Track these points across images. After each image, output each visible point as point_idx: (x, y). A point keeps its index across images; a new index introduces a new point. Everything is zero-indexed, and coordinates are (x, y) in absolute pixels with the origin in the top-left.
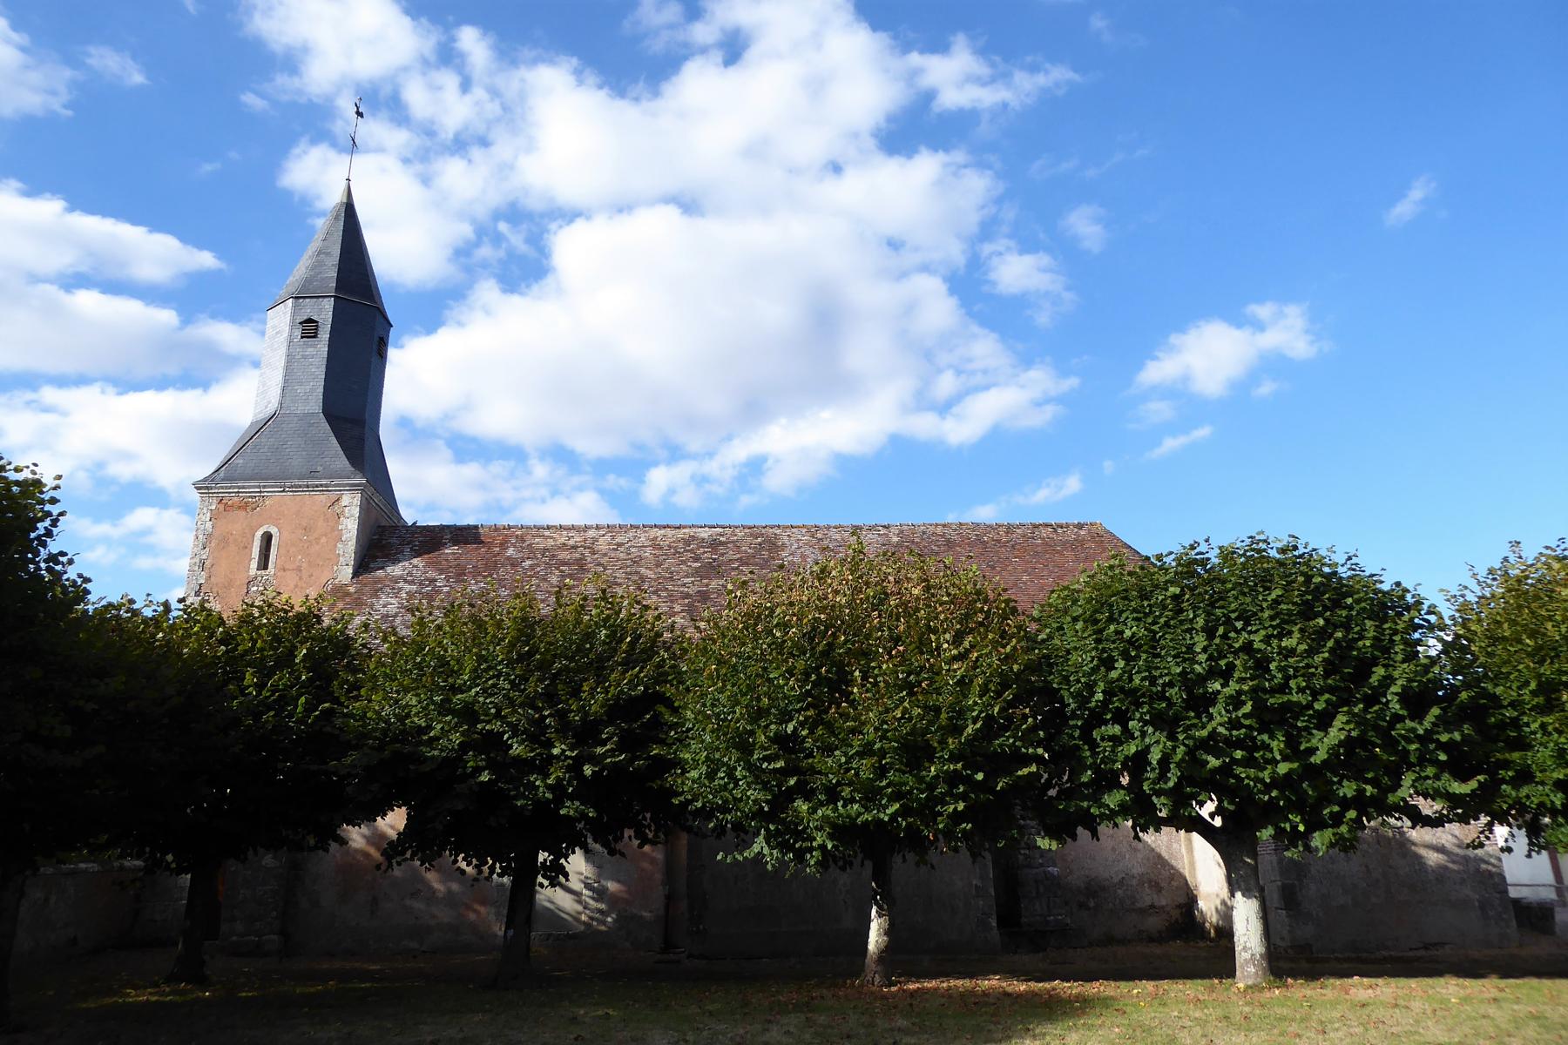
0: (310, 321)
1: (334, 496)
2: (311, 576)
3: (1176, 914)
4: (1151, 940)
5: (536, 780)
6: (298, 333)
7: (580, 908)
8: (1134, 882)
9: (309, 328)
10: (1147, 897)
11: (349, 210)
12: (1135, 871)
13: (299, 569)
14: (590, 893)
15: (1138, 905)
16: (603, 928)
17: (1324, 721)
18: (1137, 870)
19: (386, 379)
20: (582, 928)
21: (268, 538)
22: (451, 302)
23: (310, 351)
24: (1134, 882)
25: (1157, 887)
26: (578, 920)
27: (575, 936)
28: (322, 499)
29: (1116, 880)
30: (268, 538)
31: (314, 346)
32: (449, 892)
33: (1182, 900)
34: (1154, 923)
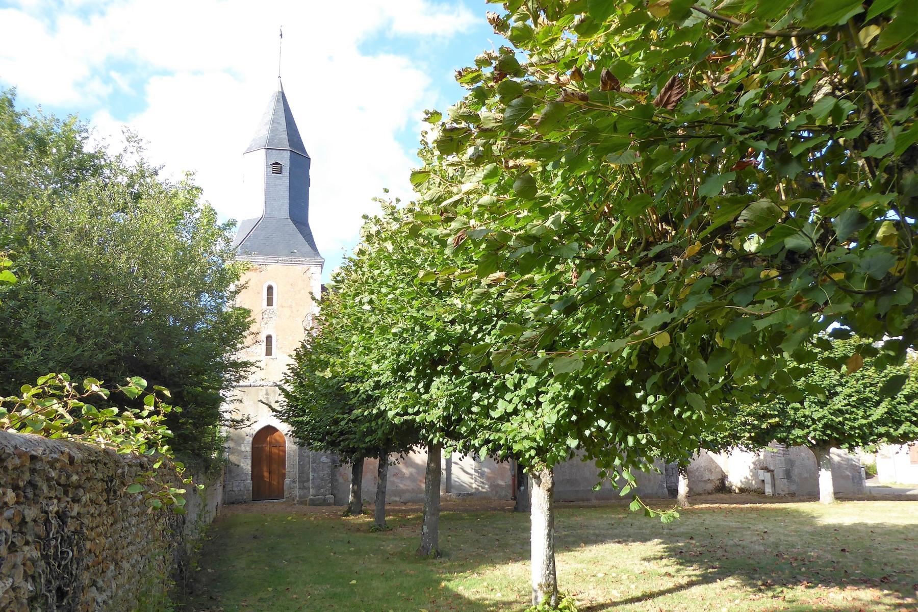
0: (277, 164)
1: (306, 267)
2: (298, 311)
3: (718, 483)
4: (709, 493)
5: (813, 155)
6: (271, 170)
7: (473, 481)
8: (702, 469)
9: (276, 167)
10: (707, 476)
11: (282, 98)
12: (702, 465)
13: (291, 307)
14: (477, 474)
15: (704, 479)
16: (484, 490)
17: (878, 404)
18: (703, 464)
19: (311, 190)
20: (474, 490)
21: (270, 288)
22: (582, 544)
23: (278, 182)
24: (702, 469)
25: (711, 471)
26: (471, 487)
27: (471, 494)
28: (300, 269)
29: (695, 468)
30: (270, 288)
31: (280, 178)
32: (411, 474)
33: (720, 477)
34: (710, 487)
